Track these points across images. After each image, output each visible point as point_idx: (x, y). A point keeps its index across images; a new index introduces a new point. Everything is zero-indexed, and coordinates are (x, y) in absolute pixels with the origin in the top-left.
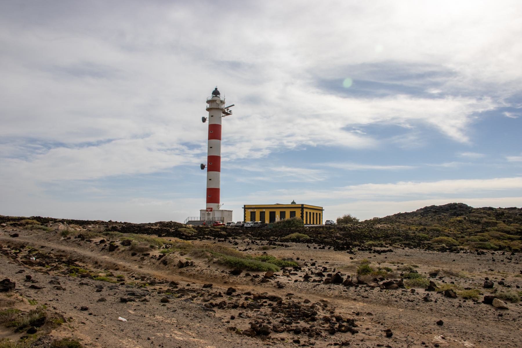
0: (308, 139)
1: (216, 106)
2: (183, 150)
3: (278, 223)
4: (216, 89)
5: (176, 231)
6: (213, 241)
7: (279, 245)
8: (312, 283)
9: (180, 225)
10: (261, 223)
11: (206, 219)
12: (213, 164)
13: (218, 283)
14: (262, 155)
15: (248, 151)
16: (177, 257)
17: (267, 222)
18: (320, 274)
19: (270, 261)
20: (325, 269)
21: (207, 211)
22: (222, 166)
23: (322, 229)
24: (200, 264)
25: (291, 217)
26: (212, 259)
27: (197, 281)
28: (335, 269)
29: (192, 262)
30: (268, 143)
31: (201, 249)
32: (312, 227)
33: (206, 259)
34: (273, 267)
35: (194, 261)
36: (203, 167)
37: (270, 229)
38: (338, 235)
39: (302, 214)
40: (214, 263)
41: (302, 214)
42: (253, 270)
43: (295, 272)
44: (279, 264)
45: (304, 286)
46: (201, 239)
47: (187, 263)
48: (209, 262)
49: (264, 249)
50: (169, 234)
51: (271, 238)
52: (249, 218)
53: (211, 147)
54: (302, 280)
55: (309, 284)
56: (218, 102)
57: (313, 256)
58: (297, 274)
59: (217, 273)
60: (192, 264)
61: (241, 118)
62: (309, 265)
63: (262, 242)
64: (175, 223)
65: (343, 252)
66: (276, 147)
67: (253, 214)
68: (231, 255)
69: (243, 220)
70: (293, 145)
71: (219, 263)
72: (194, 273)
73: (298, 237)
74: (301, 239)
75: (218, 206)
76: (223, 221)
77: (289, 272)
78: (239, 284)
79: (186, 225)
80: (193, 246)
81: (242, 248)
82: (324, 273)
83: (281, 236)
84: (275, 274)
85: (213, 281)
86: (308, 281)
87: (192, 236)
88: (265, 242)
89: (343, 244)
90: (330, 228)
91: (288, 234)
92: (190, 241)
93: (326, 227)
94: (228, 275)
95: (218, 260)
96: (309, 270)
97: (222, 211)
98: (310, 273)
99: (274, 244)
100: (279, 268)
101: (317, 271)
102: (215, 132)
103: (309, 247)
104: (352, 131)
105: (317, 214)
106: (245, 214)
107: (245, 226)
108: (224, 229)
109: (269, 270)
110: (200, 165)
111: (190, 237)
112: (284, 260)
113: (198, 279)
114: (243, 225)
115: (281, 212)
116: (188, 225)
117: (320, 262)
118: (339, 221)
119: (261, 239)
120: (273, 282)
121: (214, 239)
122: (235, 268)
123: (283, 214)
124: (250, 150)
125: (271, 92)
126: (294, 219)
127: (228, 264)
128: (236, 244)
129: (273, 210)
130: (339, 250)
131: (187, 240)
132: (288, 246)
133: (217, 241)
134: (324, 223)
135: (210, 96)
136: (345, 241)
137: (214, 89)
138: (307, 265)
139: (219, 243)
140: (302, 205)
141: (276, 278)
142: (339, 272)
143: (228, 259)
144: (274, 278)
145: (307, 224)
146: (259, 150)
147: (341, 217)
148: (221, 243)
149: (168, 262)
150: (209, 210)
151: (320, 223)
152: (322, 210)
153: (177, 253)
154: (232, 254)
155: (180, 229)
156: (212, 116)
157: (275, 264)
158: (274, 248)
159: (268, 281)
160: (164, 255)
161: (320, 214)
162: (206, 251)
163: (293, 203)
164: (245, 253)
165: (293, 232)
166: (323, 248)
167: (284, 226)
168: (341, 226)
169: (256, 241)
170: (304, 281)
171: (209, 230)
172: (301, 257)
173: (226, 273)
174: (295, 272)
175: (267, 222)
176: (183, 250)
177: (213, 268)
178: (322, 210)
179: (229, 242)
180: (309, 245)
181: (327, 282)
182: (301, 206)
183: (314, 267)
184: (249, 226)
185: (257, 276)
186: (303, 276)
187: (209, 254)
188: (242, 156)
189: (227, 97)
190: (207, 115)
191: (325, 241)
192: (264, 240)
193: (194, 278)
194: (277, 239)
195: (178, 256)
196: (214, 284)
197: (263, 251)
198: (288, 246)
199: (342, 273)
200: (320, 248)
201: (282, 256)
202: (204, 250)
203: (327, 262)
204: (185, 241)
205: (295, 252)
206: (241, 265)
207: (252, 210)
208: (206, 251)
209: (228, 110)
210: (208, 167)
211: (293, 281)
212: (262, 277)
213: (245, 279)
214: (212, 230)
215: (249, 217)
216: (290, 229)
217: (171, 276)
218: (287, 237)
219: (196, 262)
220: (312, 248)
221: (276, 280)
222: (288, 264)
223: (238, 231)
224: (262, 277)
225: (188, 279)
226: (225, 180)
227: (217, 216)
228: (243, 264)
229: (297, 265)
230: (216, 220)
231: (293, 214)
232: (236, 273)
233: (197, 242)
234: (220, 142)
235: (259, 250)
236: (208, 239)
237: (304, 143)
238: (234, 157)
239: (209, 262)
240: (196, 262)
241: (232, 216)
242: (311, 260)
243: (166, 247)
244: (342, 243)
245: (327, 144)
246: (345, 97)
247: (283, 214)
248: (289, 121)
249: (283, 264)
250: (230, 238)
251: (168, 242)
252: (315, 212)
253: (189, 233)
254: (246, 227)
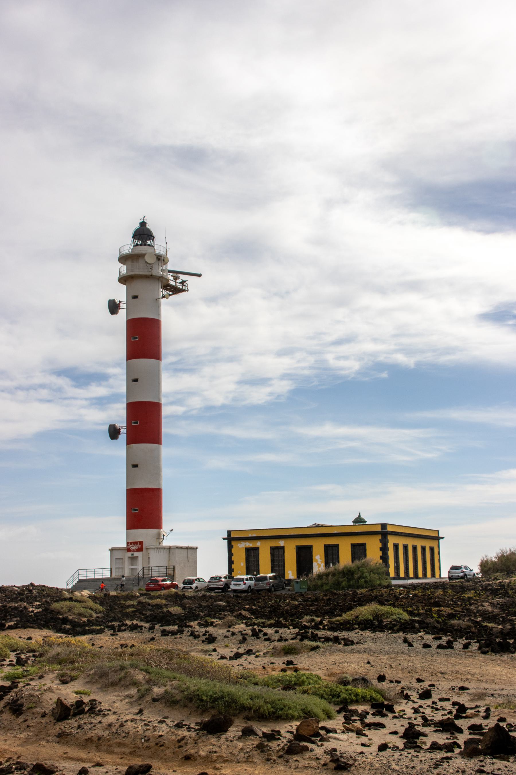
0: (393, 347)
1: (146, 268)
2: (60, 390)
3: (320, 576)
4: (143, 224)
5: (46, 610)
6: (148, 635)
7: (328, 639)
8: (428, 755)
9: (56, 594)
10: (274, 578)
11: (127, 574)
12: (143, 423)
13: (166, 760)
14: (271, 394)
15: (232, 387)
16: (50, 689)
17: (291, 574)
18: (447, 726)
19: (305, 687)
20: (462, 709)
21: (129, 550)
22: (166, 429)
23: (440, 592)
24: (116, 705)
25: (353, 559)
26: (149, 690)
27: (108, 758)
28: (488, 710)
29: (93, 702)
30: (285, 364)
31: (117, 663)
32: (414, 587)
33: (133, 691)
34: (317, 704)
35: (98, 697)
36: (114, 433)
37: (301, 595)
38: (488, 607)
39: (384, 549)
40: (154, 700)
41: (384, 549)
42: (263, 717)
43: (378, 719)
44: (332, 696)
45: (407, 762)
46: (115, 631)
47: (79, 703)
48: (141, 697)
49: (288, 651)
50: (26, 621)
51: (305, 620)
52: (243, 564)
53: (136, 380)
54: (400, 743)
55: (421, 754)
56: (149, 259)
57: (423, 669)
58: (382, 726)
59: (164, 730)
60: (93, 708)
61: (211, 300)
62: (414, 695)
63: (281, 631)
64: (42, 588)
65: (506, 657)
66: (306, 372)
67: (252, 555)
68: (201, 676)
69: (226, 573)
70: (352, 366)
71: (169, 701)
72: (100, 733)
73: (378, 616)
74: (385, 621)
75: (159, 537)
76: (172, 577)
77: (362, 720)
78: (225, 761)
79: (71, 591)
80: (95, 655)
81: (227, 652)
82: (459, 723)
83: (331, 613)
84: (323, 728)
85: (154, 756)
86: (418, 748)
87: (90, 622)
88: (289, 632)
89: (503, 634)
90: (463, 589)
91: (350, 608)
92: (84, 639)
93: (453, 587)
94: (193, 734)
95: (166, 692)
96: (416, 711)
97: (170, 548)
98: (420, 721)
99: (314, 638)
100: (333, 709)
101: (438, 717)
102: (144, 340)
103: (410, 645)
104: (511, 322)
105: (415, 548)
106: (230, 555)
107: (232, 587)
108: (178, 598)
109: (308, 715)
110: (107, 428)
111: (84, 625)
112: (344, 682)
113: (111, 752)
114: (227, 585)
115: (327, 548)
116: (77, 593)
117: (442, 687)
118: (486, 567)
119: (278, 625)
120: (318, 751)
121: (152, 628)
122: (213, 712)
123: (331, 554)
124: (240, 383)
125: (290, 225)
126: (363, 566)
127: (193, 701)
128: (211, 639)
129: (304, 542)
130: (495, 651)
131: (76, 634)
132: (352, 643)
133: (158, 635)
134: (445, 574)
135: (126, 243)
136: (508, 626)
137: (138, 225)
138: (407, 697)
139: (163, 639)
140: (384, 526)
141: (327, 740)
142: (502, 720)
143: (193, 688)
144: (322, 740)
145: (397, 577)
146: (263, 381)
147: (492, 555)
148: (169, 638)
149: (26, 706)
150: (135, 547)
151: (433, 575)
152: (438, 538)
153: (51, 676)
154: (201, 671)
155: (55, 606)
156: (135, 297)
157: (322, 697)
158: (314, 649)
159: (306, 749)
160: (15, 685)
161: (432, 549)
162: (132, 666)
163: (359, 520)
164: (236, 667)
165: (362, 601)
166: (449, 645)
167: (337, 585)
168: (494, 583)
169: (265, 630)
170: (406, 747)
171: (135, 603)
172: (389, 674)
173: (189, 729)
174: (378, 719)
175: (291, 574)
176: (68, 667)
177: (152, 716)
178: (438, 538)
179: (193, 634)
180: (410, 637)
181: (471, 751)
182: (379, 529)
183: (429, 702)
184: (242, 587)
185: (273, 736)
186: (401, 731)
187: (140, 677)
188: (219, 400)
189: (176, 249)
190: (121, 293)
191: (452, 626)
192: (285, 626)
193: (98, 749)
194: (321, 622)
195: (54, 686)
196: (155, 764)
197: (285, 659)
198: (352, 643)
199: (510, 720)
200: (440, 647)
201: (337, 670)
202: (127, 663)
203: (462, 688)
204: (72, 640)
205: (371, 659)
206: (228, 705)
207: (249, 544)
208: (132, 666)
209: (176, 278)
210: (128, 433)
211: (374, 748)
212: (289, 736)
213: (240, 745)
214: (143, 603)
215: (240, 563)
216: (355, 594)
217: (32, 748)
218: (346, 616)
219: (106, 699)
220: (418, 646)
221: (329, 745)
222: (357, 695)
223: (214, 603)
224: (289, 736)
225: (82, 754)
226: (174, 465)
227: (156, 564)
228: (234, 701)
229: (380, 699)
230: (155, 573)
231: (359, 551)
232: (216, 727)
233: (106, 640)
234: (159, 366)
235: (273, 655)
236: (133, 628)
237: (381, 358)
238: (196, 402)
239: (141, 697)
240: (106, 699)
241: (195, 562)
242: (419, 680)
243: (20, 662)
244: (501, 632)
245: (444, 359)
246: (488, 232)
247: (331, 554)
248: (341, 302)
249: (344, 695)
250: (194, 624)
251: (22, 643)
252: (419, 543)
253: (81, 615)
254: (235, 591)
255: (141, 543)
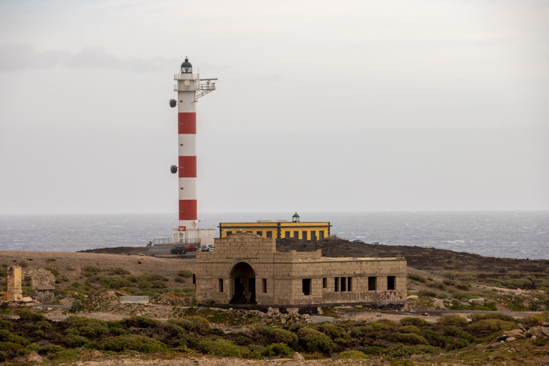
4: (187, 60)
21: (179, 230)
102: (187, 123)
137: (184, 61)
140: (279, 224)
182: (276, 225)
190: (175, 96)
207: (228, 230)
255: (185, 227)
